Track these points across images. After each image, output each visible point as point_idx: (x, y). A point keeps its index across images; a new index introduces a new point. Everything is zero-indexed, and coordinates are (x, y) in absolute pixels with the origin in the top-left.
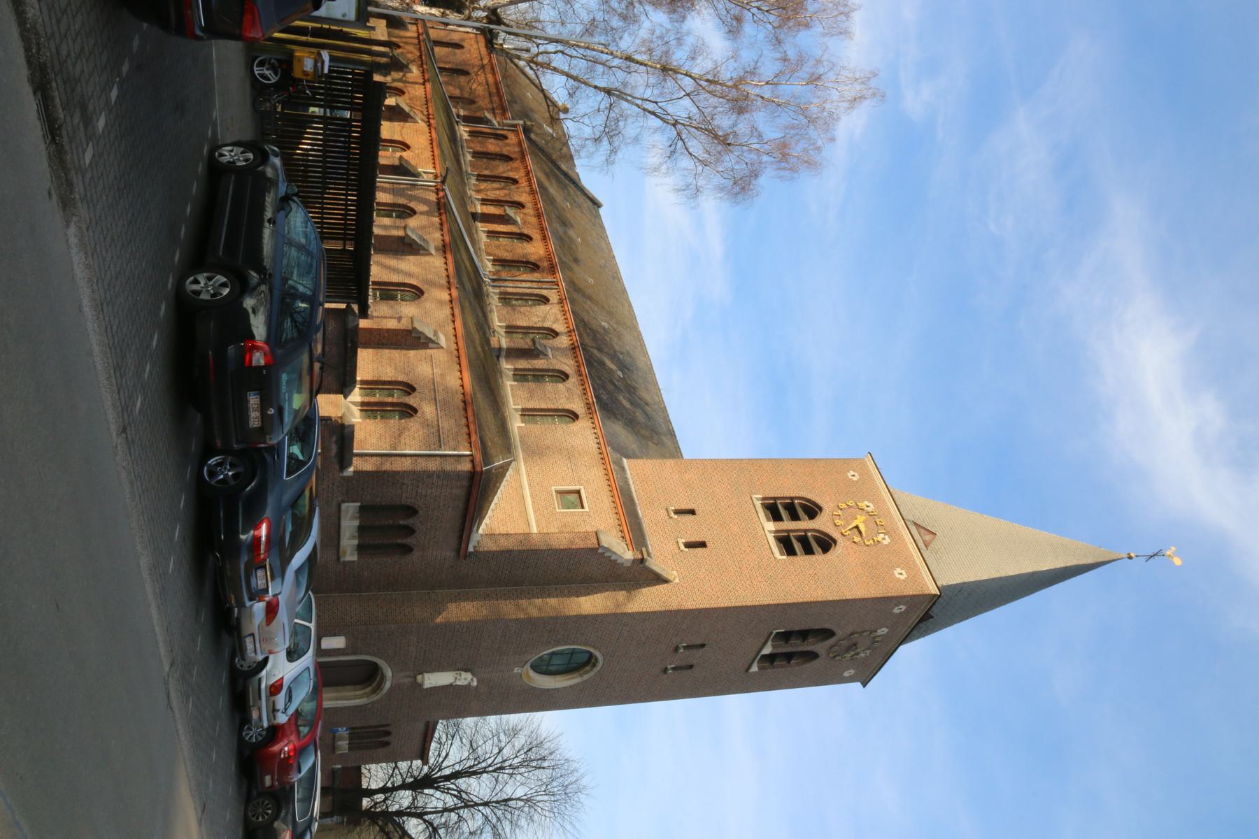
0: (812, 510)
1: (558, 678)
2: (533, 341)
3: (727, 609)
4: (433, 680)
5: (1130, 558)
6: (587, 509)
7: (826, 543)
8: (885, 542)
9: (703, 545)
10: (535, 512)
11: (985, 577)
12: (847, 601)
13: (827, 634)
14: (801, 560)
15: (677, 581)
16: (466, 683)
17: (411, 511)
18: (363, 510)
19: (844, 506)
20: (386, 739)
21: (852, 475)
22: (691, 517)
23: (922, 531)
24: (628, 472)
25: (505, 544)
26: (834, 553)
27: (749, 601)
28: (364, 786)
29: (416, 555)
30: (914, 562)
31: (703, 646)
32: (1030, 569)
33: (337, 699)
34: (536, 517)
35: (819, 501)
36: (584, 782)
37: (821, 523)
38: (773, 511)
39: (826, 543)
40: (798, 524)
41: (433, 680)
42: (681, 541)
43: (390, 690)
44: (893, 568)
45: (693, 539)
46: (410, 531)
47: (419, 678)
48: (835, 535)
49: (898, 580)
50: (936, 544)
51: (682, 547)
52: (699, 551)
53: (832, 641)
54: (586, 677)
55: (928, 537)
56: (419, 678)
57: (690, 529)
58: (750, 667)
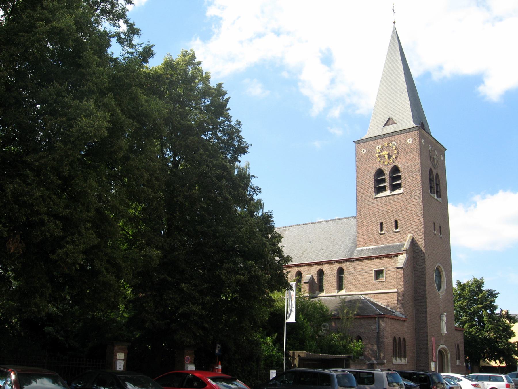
0: (380, 172)
1: (442, 280)
2: (305, 283)
7: (395, 170)
8: (395, 144)
9: (396, 222)
10: (385, 289)
11: (408, 99)
12: (421, 166)
13: (431, 171)
17: (395, 338)
18: (395, 356)
20: (397, 339)
22: (384, 225)
23: (388, 123)
24: (365, 248)
29: (406, 337)
31: (434, 223)
32: (403, 76)
33: (448, 365)
35: (376, 169)
37: (387, 171)
38: (379, 190)
39: (395, 170)
40: (386, 180)
42: (394, 230)
43: (446, 345)
46: (399, 338)
48: (392, 165)
49: (412, 142)
51: (397, 230)
52: (399, 224)
53: (433, 169)
54: (443, 269)
55: (390, 122)
57: (389, 226)
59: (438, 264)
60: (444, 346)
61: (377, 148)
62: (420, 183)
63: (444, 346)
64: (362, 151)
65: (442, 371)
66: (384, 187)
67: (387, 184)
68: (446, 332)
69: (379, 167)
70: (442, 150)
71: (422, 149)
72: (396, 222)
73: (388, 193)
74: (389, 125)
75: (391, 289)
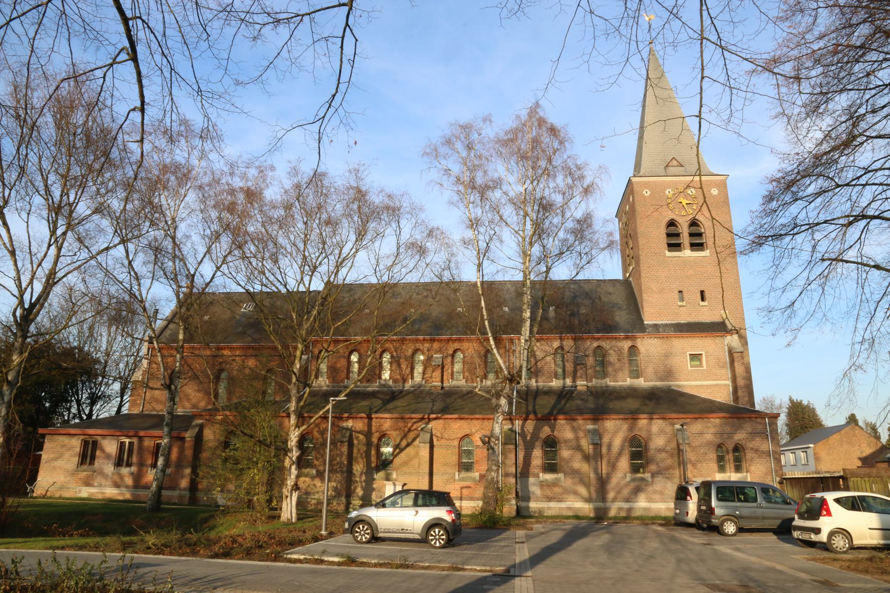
9: (702, 292)
35: (667, 219)
72: (702, 292)
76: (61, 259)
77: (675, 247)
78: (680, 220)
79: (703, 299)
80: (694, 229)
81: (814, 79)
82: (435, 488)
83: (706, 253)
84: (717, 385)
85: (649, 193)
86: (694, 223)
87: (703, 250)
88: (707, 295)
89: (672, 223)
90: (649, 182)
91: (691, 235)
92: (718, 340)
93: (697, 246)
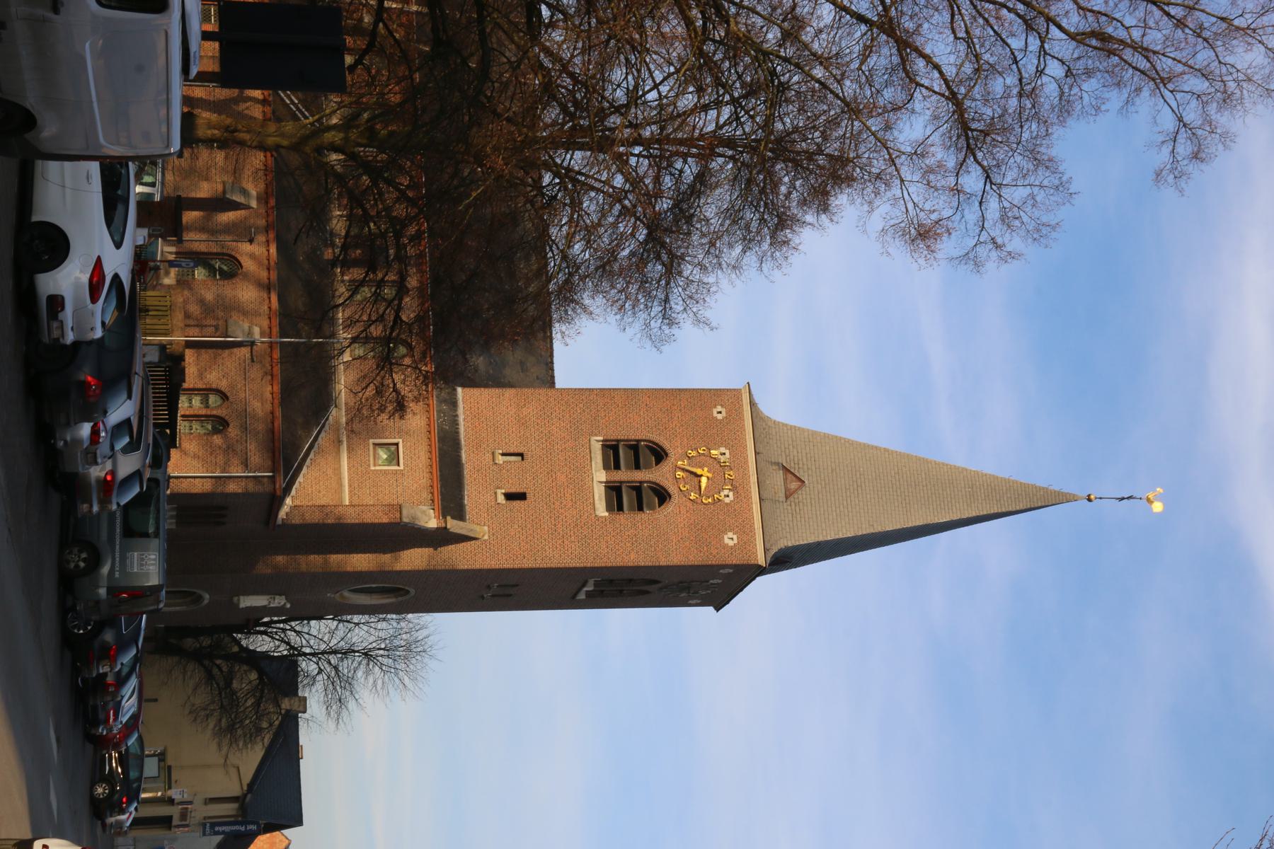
1: (374, 596)
3: (532, 569)
4: (247, 602)
5: (1089, 500)
6: (402, 467)
9: (521, 496)
12: (660, 567)
13: (656, 582)
14: (627, 519)
15: (486, 537)
16: (264, 649)
19: (694, 453)
21: (719, 413)
24: (461, 411)
25: (314, 518)
26: (669, 508)
27: (554, 563)
28: (217, 45)
30: (752, 525)
34: (349, 475)
35: (666, 445)
36: (430, 641)
41: (247, 602)
44: (725, 532)
45: (513, 490)
47: (235, 599)
50: (802, 495)
51: (501, 499)
52: (517, 504)
53: (660, 585)
54: (400, 599)
56: (235, 599)
58: (576, 594)
59: (412, 591)
60: (206, 602)
61: (723, 450)
62: (618, 562)
63: (206, 602)
64: (719, 408)
65: (145, 290)
66: (617, 467)
67: (624, 475)
68: (242, 605)
69: (671, 453)
70: (719, 603)
71: (712, 570)
72: (521, 496)
73: (600, 476)
74: (785, 480)
75: (350, 486)
76: (1131, 71)
77: (612, 451)
78: (666, 466)
79: (510, 497)
80: (647, 495)
81: (647, 88)
82: (146, 760)
83: (602, 511)
84: (341, 485)
85: (720, 417)
86: (662, 496)
87: (609, 508)
88: (517, 504)
89: (659, 455)
90: (742, 419)
91: (637, 489)
92: (426, 495)
93: (614, 492)
